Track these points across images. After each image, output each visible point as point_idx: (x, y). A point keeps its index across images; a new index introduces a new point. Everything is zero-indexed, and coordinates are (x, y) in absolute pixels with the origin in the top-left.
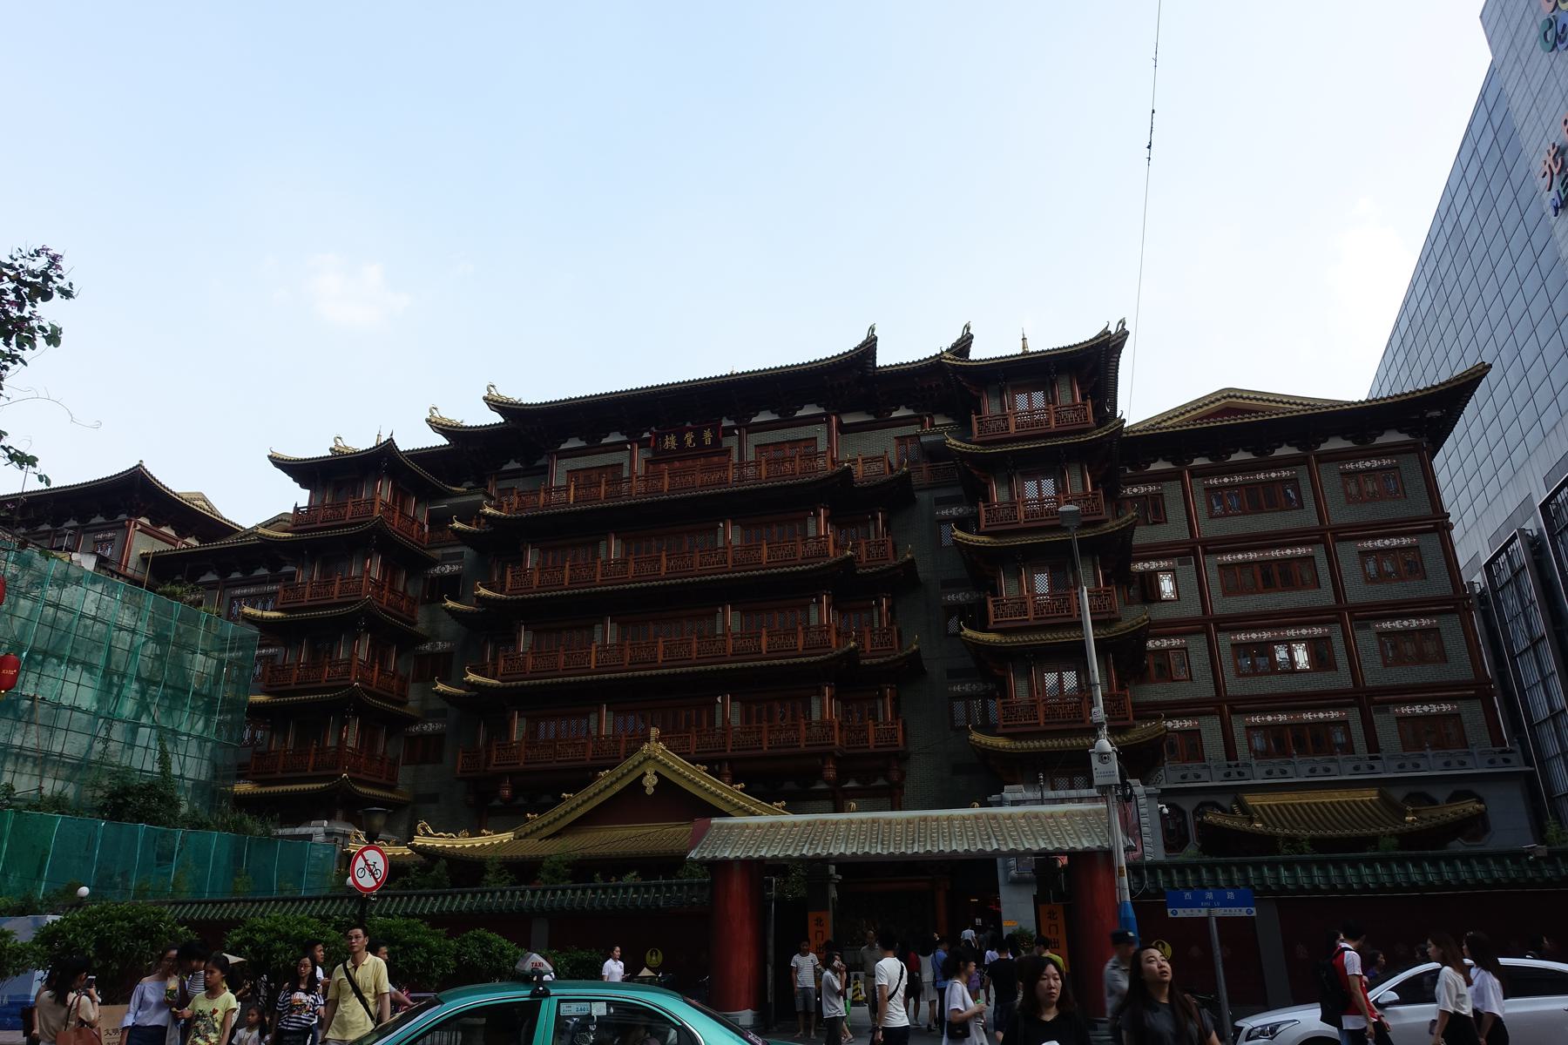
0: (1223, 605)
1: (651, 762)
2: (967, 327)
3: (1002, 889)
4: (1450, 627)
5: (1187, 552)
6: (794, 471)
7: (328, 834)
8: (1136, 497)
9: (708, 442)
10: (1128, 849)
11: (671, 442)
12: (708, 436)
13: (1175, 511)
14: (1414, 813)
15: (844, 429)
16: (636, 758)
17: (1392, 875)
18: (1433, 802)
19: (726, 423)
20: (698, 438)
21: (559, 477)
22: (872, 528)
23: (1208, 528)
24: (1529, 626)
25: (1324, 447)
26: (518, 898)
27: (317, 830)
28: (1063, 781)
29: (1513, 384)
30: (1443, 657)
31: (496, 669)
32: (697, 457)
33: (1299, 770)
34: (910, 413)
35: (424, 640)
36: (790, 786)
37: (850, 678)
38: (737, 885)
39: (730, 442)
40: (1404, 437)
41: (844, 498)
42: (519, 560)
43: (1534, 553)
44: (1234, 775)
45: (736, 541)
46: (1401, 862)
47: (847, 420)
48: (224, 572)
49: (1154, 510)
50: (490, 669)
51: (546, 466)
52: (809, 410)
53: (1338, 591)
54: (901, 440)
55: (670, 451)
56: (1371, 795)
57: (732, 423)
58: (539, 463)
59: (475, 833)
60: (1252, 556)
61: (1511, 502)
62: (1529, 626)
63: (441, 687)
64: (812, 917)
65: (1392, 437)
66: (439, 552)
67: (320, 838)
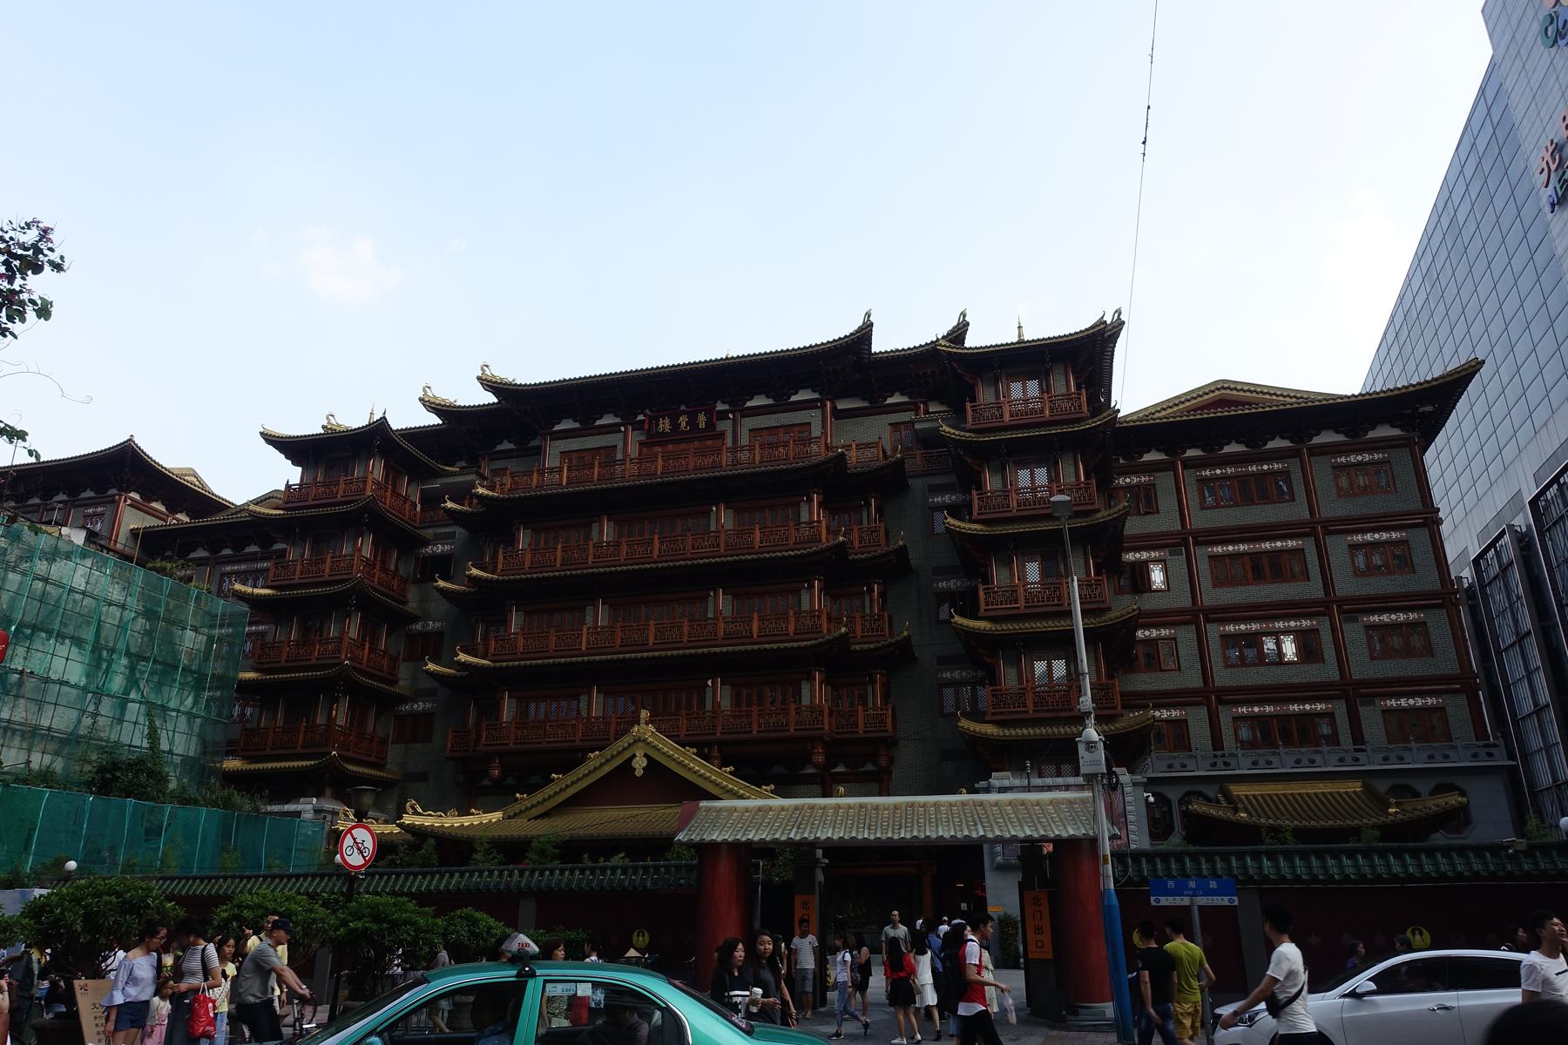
0: (1212, 596)
2: (963, 314)
3: (988, 875)
4: (1437, 622)
5: (1177, 542)
6: (787, 457)
7: (317, 811)
9: (702, 425)
10: (1113, 838)
11: (664, 425)
12: (702, 420)
13: (1167, 502)
14: (1397, 805)
15: (839, 415)
16: (627, 739)
17: (1373, 867)
18: (1417, 795)
19: (720, 407)
20: (693, 422)
23: (1200, 519)
24: (1516, 622)
25: (1316, 440)
27: (306, 807)
28: (1052, 768)
29: (1505, 380)
30: (1429, 651)
34: (905, 399)
35: (414, 619)
36: (778, 769)
37: (841, 664)
38: (724, 867)
39: (725, 426)
40: (1396, 432)
41: (838, 484)
42: (511, 541)
43: (1522, 549)
46: (1383, 854)
47: (842, 405)
48: (214, 549)
49: (1146, 500)
50: (481, 649)
51: (539, 448)
53: (1327, 583)
55: (663, 434)
56: (1355, 787)
57: (726, 407)
58: (532, 444)
59: (464, 812)
60: (1243, 547)
61: (1500, 498)
62: (1516, 622)
63: (431, 666)
64: (798, 900)
65: (1384, 432)
66: (431, 531)
67: (308, 816)
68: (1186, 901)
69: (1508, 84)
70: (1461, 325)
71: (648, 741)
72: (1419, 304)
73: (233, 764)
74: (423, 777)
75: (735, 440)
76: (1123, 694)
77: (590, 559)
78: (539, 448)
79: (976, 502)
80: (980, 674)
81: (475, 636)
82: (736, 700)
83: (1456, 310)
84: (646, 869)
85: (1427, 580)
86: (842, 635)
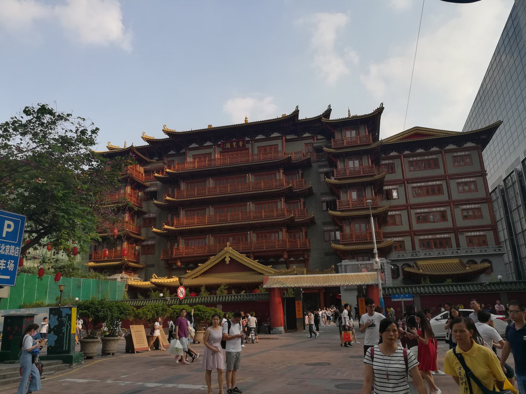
0: (413, 201)
1: (228, 253)
2: (330, 106)
3: (341, 292)
4: (485, 207)
5: (403, 182)
6: (270, 157)
7: (122, 278)
8: (385, 164)
9: (241, 145)
10: (382, 284)
11: (228, 145)
12: (241, 143)
13: (398, 170)
14: (469, 266)
15: (287, 141)
16: (223, 252)
17: (449, 289)
18: (476, 263)
20: (238, 144)
21: (190, 159)
22: (297, 176)
23: (409, 175)
24: (517, 201)
25: (447, 148)
26: (212, 299)
27: (118, 277)
28: (361, 258)
29: (516, 118)
30: (481, 217)
31: (173, 223)
32: (236, 151)
33: (435, 253)
34: (310, 135)
35: (145, 213)
36: (272, 260)
37: (291, 226)
38: (277, 293)
39: (248, 146)
40: (473, 145)
41: (289, 166)
42: (179, 187)
43: (519, 177)
44: (415, 255)
45: (253, 181)
46: (452, 286)
47: (288, 137)
49: (391, 169)
50: (170, 223)
51: (185, 153)
52: (275, 135)
53: (449, 195)
54: (306, 144)
55: (228, 149)
56: (457, 261)
57: (249, 139)
58: (181, 152)
59: (169, 277)
60: (422, 184)
61: (513, 159)
62: (517, 201)
63: (154, 230)
64: (296, 302)
65: (469, 144)
66: (149, 183)
67: (119, 280)
68: (400, 300)
69: (520, 14)
70: (502, 97)
71: (230, 252)
72: (495, 74)
73: (92, 264)
74: (153, 266)
75: (253, 152)
76: (383, 233)
77: (207, 193)
78: (185, 153)
79: (335, 171)
80: (337, 228)
81: (168, 219)
82: (258, 237)
83: (500, 92)
84: (253, 295)
85: (481, 194)
86: (292, 217)
